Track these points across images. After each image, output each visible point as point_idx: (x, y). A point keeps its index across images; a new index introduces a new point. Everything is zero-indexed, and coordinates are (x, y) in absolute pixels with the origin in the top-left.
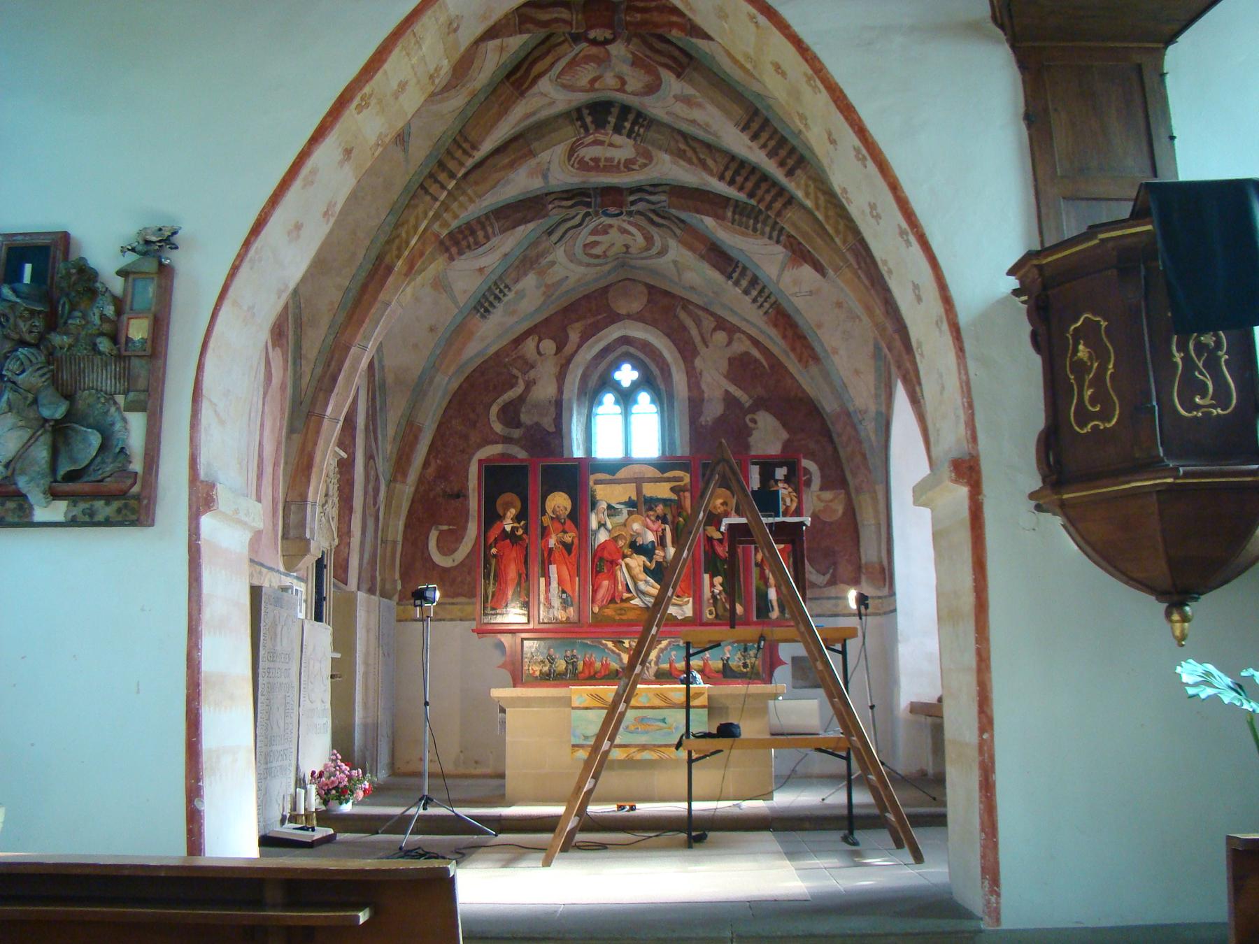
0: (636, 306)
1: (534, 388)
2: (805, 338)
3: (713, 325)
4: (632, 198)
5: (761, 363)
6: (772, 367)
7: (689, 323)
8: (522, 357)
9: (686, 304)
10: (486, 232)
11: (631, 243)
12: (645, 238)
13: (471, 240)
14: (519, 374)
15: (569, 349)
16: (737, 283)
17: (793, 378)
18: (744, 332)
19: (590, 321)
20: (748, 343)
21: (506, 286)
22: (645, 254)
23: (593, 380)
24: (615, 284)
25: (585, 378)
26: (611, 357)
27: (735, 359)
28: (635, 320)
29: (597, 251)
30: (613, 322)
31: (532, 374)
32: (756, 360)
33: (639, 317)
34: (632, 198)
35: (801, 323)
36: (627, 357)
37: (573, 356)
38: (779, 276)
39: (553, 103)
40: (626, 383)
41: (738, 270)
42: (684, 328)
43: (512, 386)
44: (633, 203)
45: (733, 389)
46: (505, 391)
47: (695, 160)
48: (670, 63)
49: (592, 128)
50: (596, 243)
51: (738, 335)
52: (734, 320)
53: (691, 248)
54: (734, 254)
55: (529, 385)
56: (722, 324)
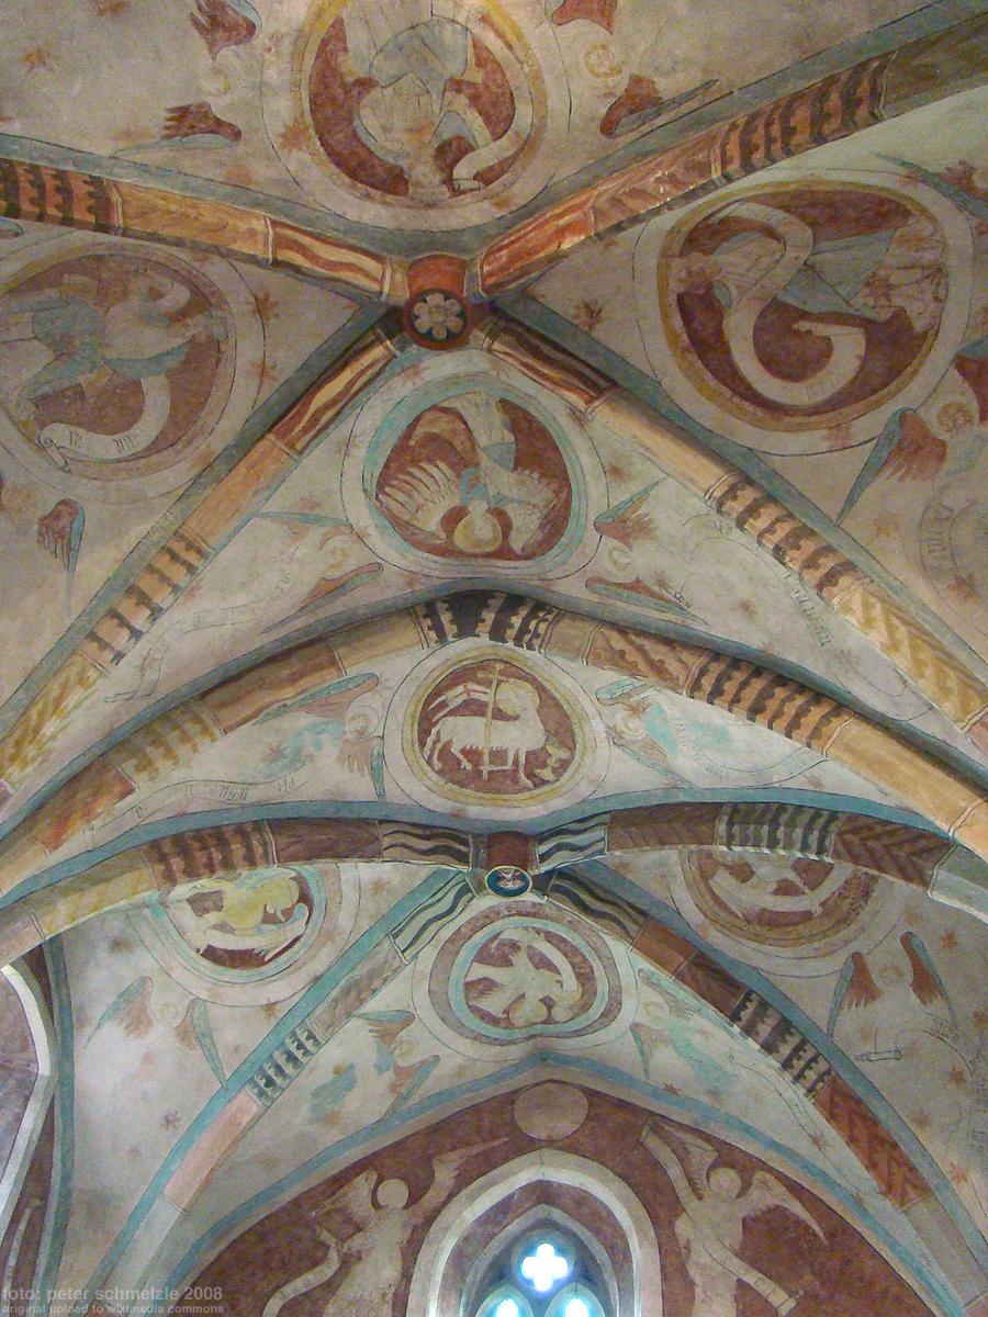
0: (565, 1126)
1: (358, 1268)
2: (895, 1146)
3: (711, 1156)
4: (543, 848)
5: (807, 1228)
6: (831, 1235)
7: (664, 1154)
8: (343, 1211)
9: (658, 1123)
10: (249, 848)
11: (555, 993)
12: (579, 976)
13: (217, 856)
14: (332, 1241)
15: (432, 1197)
16: (749, 1030)
17: (876, 1254)
18: (770, 1170)
19: (476, 1150)
20: (780, 1189)
21: (311, 1036)
22: (582, 1021)
23: (476, 1274)
24: (527, 1088)
25: (460, 1259)
26: (514, 1227)
27: (756, 1219)
28: (561, 1149)
29: (494, 1004)
30: (520, 1152)
31: (357, 1242)
32: (798, 1222)
33: (571, 1146)
34: (543, 848)
35: (881, 1114)
36: (547, 1228)
37: (437, 1211)
38: (832, 1022)
39: (375, 568)
40: (542, 1285)
41: (751, 1007)
42: (656, 1165)
43: (315, 1263)
44: (544, 857)
45: (752, 1278)
46: (299, 1273)
47: (642, 666)
48: (575, 382)
49: (451, 629)
50: (487, 986)
51: (759, 1175)
52: (752, 1148)
53: (660, 961)
54: (740, 976)
55: (348, 1262)
56: (727, 1156)
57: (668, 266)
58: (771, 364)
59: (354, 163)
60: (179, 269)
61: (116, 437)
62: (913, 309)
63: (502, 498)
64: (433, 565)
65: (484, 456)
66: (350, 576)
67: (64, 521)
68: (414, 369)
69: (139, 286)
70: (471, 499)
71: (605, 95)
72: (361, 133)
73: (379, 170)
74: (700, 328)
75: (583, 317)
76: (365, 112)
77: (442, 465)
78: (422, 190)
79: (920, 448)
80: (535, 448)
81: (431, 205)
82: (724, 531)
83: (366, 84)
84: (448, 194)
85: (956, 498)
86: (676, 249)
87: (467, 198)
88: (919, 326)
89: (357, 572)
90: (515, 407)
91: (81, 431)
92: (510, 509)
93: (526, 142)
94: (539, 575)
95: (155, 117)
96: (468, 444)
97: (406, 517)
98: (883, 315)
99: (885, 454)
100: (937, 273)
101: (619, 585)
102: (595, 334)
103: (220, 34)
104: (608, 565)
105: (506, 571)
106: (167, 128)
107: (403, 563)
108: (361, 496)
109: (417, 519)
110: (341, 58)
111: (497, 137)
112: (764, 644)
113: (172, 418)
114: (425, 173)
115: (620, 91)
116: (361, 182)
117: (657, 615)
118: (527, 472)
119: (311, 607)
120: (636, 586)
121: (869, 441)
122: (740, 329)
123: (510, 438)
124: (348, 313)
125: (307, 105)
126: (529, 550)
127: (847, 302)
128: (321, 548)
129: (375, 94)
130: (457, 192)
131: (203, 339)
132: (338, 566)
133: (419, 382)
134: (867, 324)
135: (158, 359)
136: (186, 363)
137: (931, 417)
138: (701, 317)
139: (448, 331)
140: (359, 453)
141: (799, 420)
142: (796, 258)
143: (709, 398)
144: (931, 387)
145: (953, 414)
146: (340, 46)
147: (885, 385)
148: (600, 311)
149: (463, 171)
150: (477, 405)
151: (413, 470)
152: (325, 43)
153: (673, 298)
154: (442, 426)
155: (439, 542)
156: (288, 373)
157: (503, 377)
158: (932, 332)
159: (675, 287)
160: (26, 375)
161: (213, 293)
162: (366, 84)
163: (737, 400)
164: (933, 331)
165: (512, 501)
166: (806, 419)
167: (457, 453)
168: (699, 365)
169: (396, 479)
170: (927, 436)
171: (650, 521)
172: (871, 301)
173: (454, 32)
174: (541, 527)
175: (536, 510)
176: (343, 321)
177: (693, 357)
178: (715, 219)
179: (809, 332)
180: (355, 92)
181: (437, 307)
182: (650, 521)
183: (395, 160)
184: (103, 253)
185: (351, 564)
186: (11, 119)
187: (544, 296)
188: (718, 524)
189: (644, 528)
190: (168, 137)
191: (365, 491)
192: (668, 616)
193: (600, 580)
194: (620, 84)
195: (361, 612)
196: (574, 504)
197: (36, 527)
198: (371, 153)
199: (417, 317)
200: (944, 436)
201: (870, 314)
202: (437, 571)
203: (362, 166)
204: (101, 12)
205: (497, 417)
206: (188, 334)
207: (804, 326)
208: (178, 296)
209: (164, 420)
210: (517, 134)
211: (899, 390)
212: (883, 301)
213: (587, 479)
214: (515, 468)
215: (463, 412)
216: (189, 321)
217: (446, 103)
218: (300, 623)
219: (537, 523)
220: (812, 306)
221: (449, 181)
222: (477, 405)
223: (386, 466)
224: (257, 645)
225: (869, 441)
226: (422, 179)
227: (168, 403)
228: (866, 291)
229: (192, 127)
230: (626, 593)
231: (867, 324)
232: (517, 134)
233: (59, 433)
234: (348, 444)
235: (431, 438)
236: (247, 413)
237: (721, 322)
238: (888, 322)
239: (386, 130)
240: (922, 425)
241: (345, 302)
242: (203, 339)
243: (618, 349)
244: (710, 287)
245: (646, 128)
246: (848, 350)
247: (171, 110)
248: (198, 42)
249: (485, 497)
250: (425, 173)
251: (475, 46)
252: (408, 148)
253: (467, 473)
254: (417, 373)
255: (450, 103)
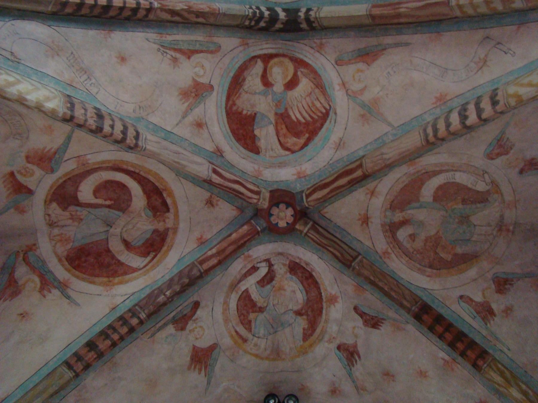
39: (339, 62)
57: (174, 224)
58: (122, 186)
59: (310, 281)
60: (398, 249)
61: (454, 181)
62: (59, 211)
63: (265, 94)
64: (308, 55)
65: (271, 119)
66: (353, 61)
67: (497, 151)
68: (300, 176)
69: (419, 244)
70: (281, 93)
71: (197, 319)
72: (304, 292)
73: (300, 275)
74: (158, 199)
75: (214, 202)
76: (301, 301)
77: (294, 118)
78: (282, 261)
79: (40, 160)
80: (243, 128)
81: (281, 254)
82: (138, 107)
83: (298, 313)
84: (272, 259)
85: (14, 144)
86: (170, 233)
87: (264, 258)
88: (54, 205)
89: (349, 62)
90: (251, 151)
91: (470, 186)
92: (260, 87)
93: (234, 289)
94: (248, 47)
95: (386, 328)
96: (279, 128)
97: (317, 90)
98: (72, 208)
99: (57, 156)
100: (52, 225)
101: (202, 52)
102: (209, 194)
103: (351, 349)
104: (207, 65)
105: (268, 46)
106: (382, 323)
107: (323, 60)
108: (338, 111)
109: (312, 88)
110: (306, 326)
111: (246, 291)
112: (110, 37)
113: (423, 184)
114: (280, 269)
115: (190, 323)
116: (308, 271)
117: (178, 37)
118: (249, 113)
119: (380, 48)
120: (189, 54)
121: (68, 160)
122: (138, 197)
123: (257, 132)
124: (325, 210)
125: (324, 311)
126: (252, 63)
127: (89, 212)
128: (366, 87)
129: (296, 308)
130: (268, 261)
131: (397, 211)
132: (359, 71)
133: (298, 168)
134: (79, 204)
135: (421, 207)
136: (409, 203)
137: (38, 172)
138: (158, 203)
139: (278, 207)
140: (334, 138)
141: (104, 165)
142: (116, 229)
143: (151, 171)
144: (43, 183)
145: (27, 173)
146: (305, 331)
147: (65, 181)
148: (206, 204)
149: (263, 271)
150: (272, 150)
151: (309, 119)
152: (311, 335)
153: (172, 210)
154: (291, 141)
155: (302, 70)
156: (361, 190)
157: (256, 167)
158: (48, 203)
159: (171, 215)
160: (486, 212)
161: (386, 231)
162: (298, 313)
163: (137, 171)
164: (47, 202)
165: (259, 94)
166: (101, 166)
167: (285, 123)
168: (157, 184)
169: (318, 116)
170: (38, 165)
171: (181, 100)
172: (79, 213)
173: (259, 333)
174: (244, 80)
175: (246, 90)
176: (329, 207)
177: (160, 187)
178: (152, 255)
179: (105, 200)
180: (304, 311)
181: (282, 219)
182: (181, 100)
183: (292, 278)
184: (429, 270)
185: (351, 69)
186: (442, 359)
187: (233, 210)
188: (142, 111)
189: (185, 94)
190: (383, 319)
191: (336, 114)
192: (170, 38)
193: (212, 52)
194: (190, 325)
195: (352, 33)
196: (224, 99)
197: (512, 151)
198: (302, 283)
199: (292, 216)
200: (29, 165)
201: (78, 208)
202: (305, 51)
203: (307, 278)
204: (393, 376)
205: (262, 144)
206: (404, 213)
207: (108, 203)
208: (402, 234)
209: (427, 183)
210: (237, 293)
211: (58, 180)
212: (74, 213)
213: (216, 117)
214: (255, 114)
215: (279, 147)
216: (401, 219)
217: (267, 302)
218: (389, 40)
219: (247, 82)
220: (107, 210)
221: (270, 265)
222: (272, 150)
223: (322, 125)
224: (417, 37)
225: (68, 160)
226: (282, 267)
227: (423, 190)
228: (82, 217)
229: (372, 319)
230: (198, 47)
231: (79, 204)
232: (237, 293)
233: (481, 187)
234: (340, 145)
235: (297, 135)
236: (385, 178)
237: (148, 203)
238: (69, 205)
239: (294, 292)
240: (43, 169)
241: (326, 215)
242: (397, 211)
243: (198, 188)
244: (154, 216)
245: (179, 309)
246: (86, 191)
247: (378, 329)
248: (361, 350)
249: (274, 93)
250: (280, 269)
251: (251, 329)
252: (286, 282)
253: (281, 111)
254: (299, 173)
255: (264, 302)
